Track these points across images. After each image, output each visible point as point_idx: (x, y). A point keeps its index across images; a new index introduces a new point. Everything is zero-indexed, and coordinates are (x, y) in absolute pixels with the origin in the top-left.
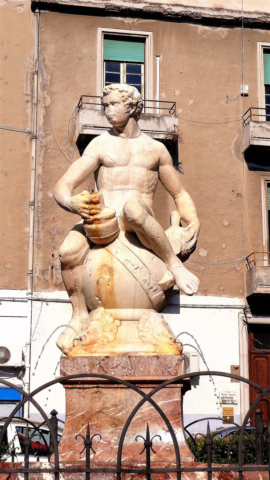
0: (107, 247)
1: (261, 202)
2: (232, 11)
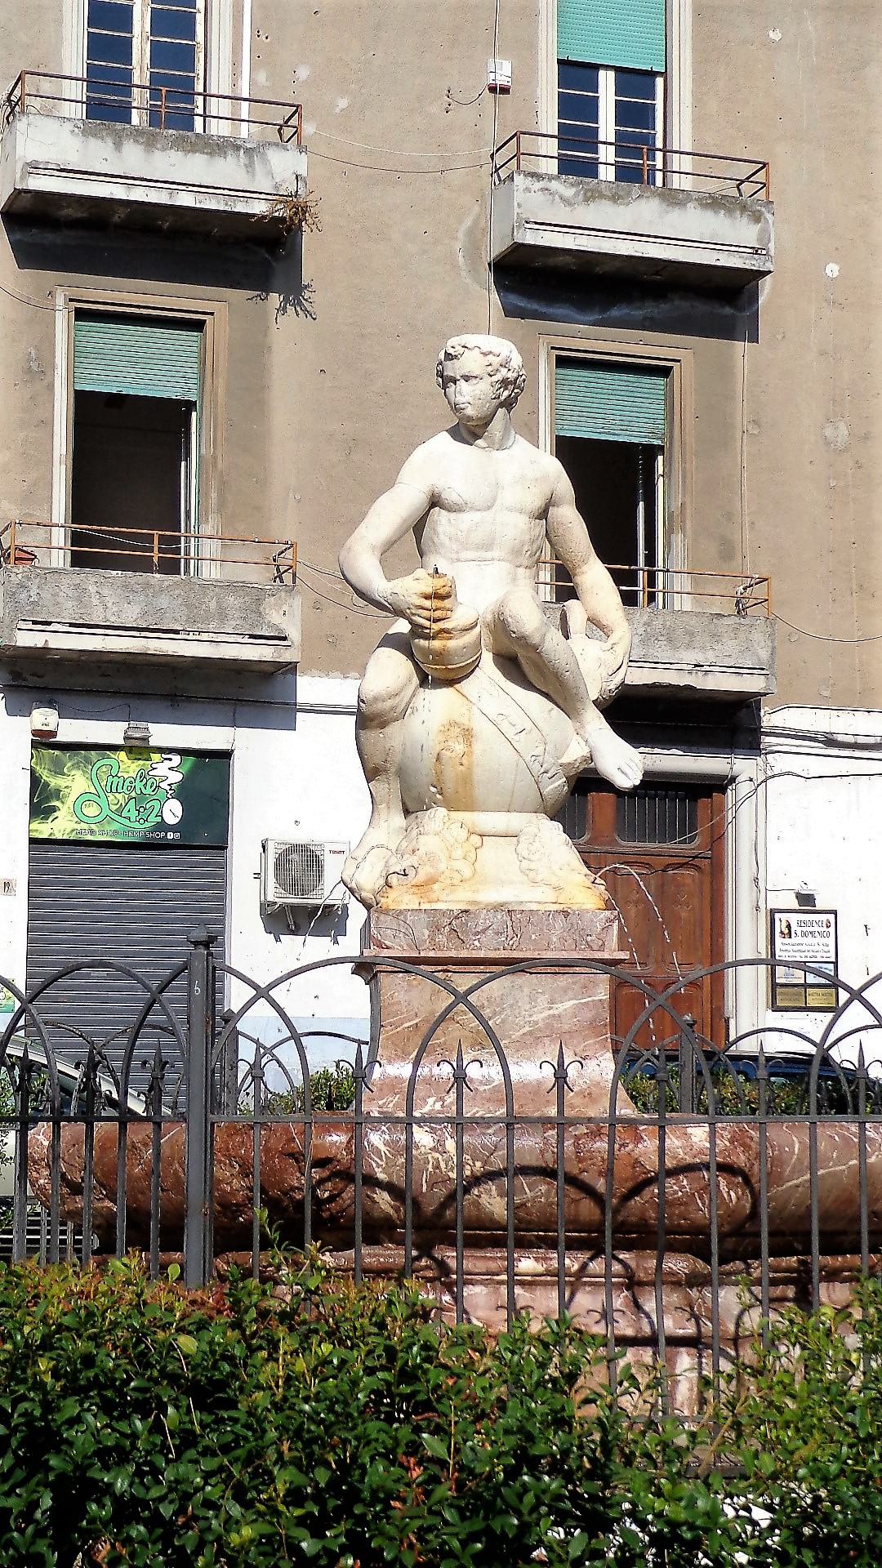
0: (457, 686)
1: (536, 412)
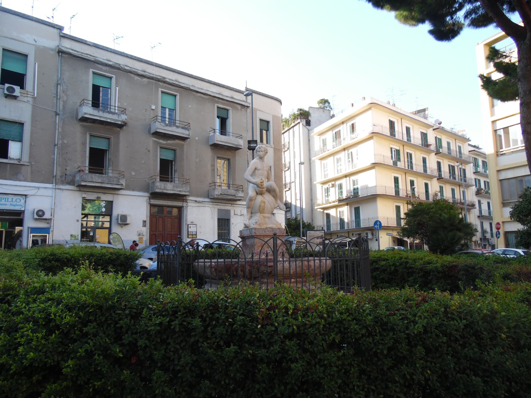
2: (150, 74)
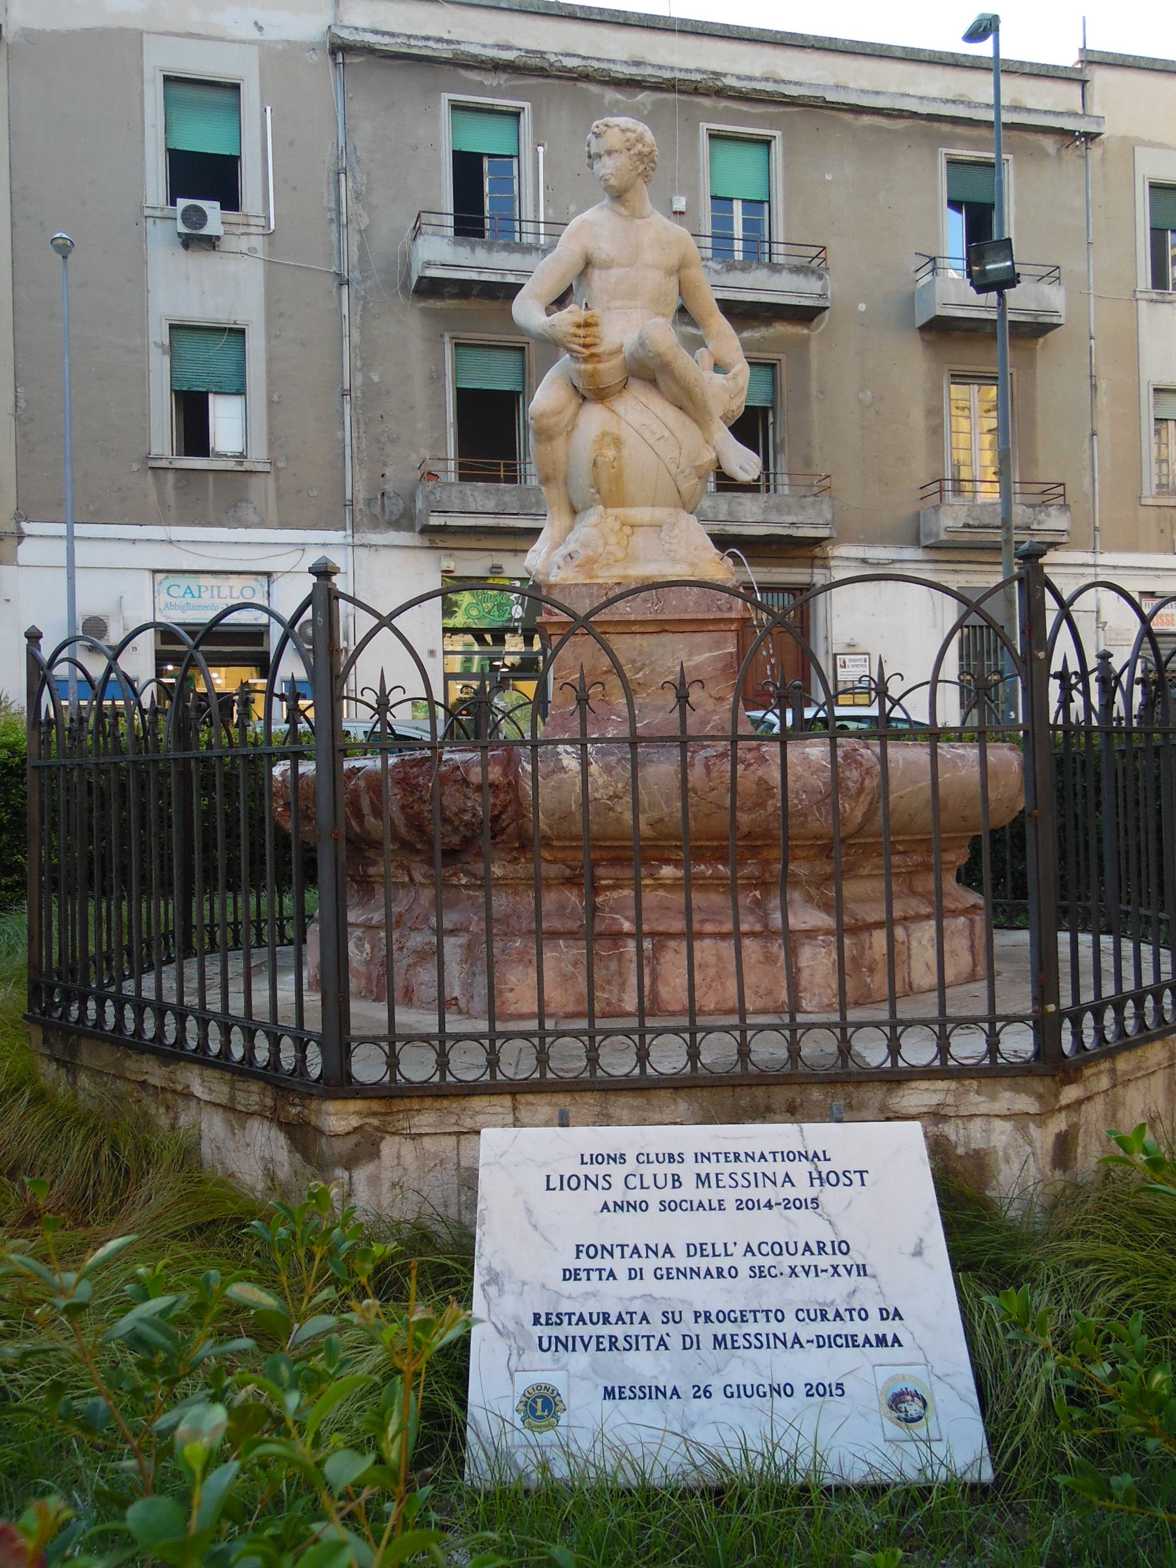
2: (660, 67)
